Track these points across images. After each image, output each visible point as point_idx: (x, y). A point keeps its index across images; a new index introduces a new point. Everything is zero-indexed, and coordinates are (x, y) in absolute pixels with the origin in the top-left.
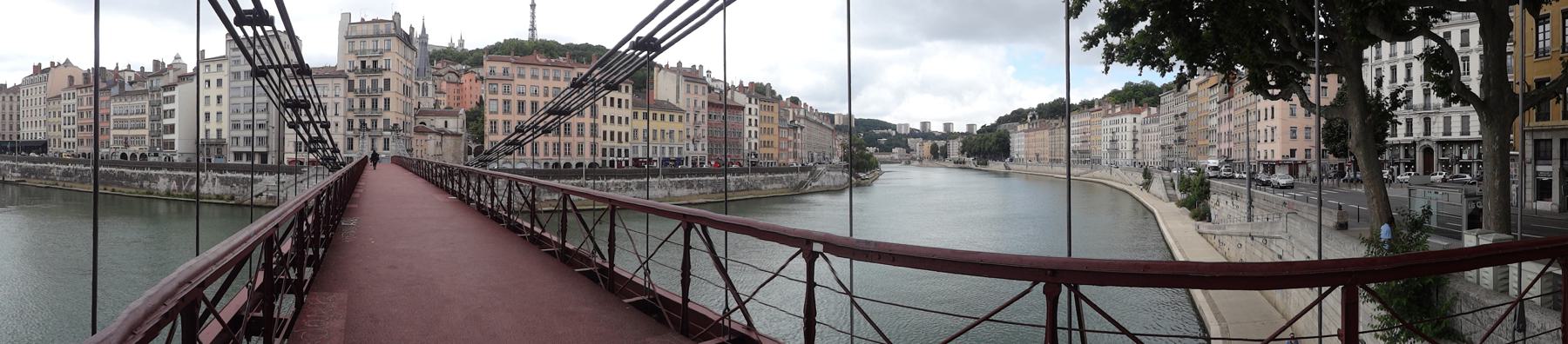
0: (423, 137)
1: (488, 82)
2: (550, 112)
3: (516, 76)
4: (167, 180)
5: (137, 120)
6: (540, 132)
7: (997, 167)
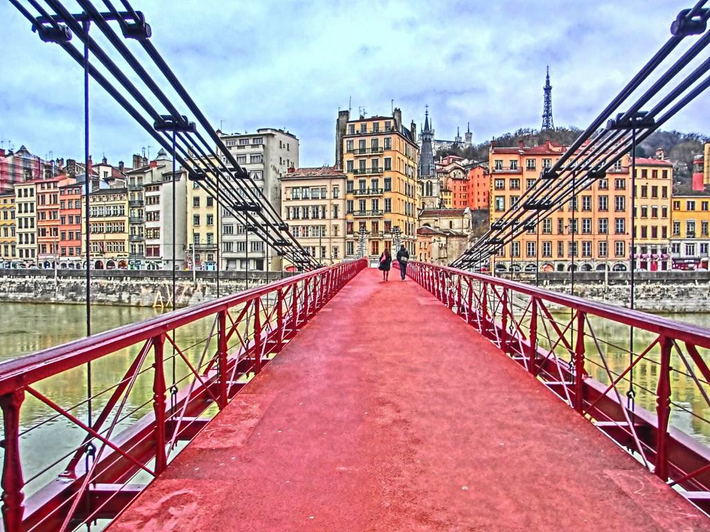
0: (427, 240)
1: (494, 177)
2: (527, 207)
3: (525, 169)
4: (150, 290)
5: (115, 222)
6: (521, 229)
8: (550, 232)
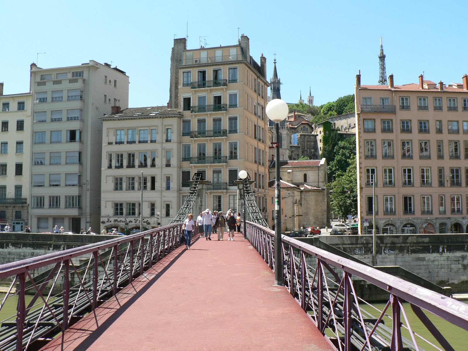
3: (398, 107)
7: (454, 306)
8: (430, 185)
